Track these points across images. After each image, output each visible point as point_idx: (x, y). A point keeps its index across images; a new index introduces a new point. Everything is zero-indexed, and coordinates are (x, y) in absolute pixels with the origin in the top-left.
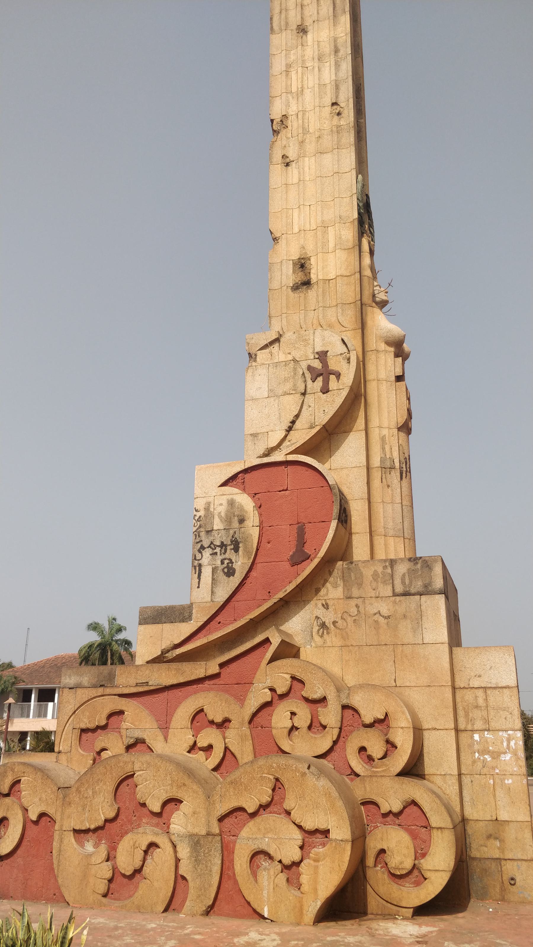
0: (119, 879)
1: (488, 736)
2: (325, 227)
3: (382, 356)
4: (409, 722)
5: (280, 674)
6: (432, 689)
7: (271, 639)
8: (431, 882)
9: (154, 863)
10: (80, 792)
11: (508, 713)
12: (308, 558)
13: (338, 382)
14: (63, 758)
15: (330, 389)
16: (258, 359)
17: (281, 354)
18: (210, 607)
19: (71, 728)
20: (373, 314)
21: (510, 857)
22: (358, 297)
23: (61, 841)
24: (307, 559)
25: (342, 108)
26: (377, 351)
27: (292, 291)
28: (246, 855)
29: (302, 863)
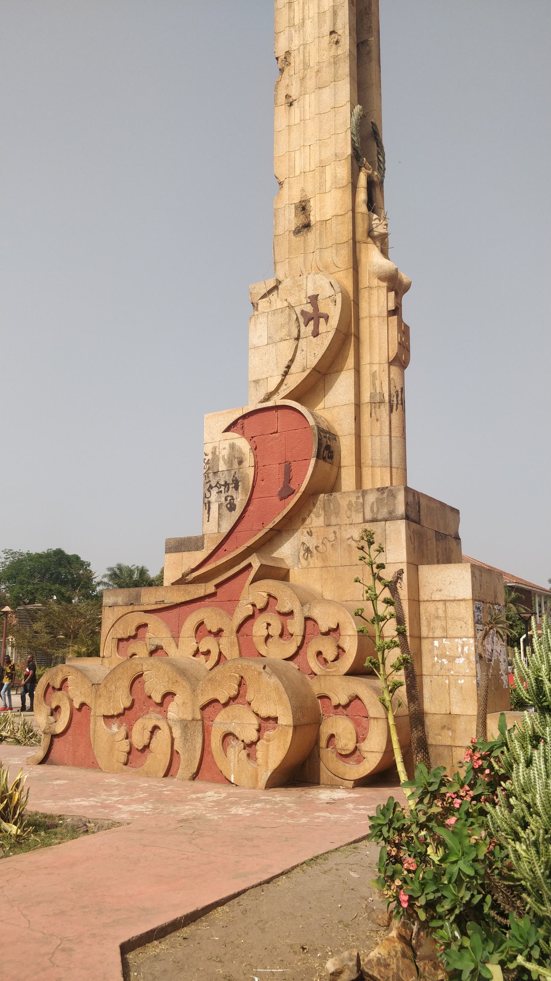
0: (135, 752)
1: (446, 642)
2: (322, 166)
3: (375, 292)
7: (252, 564)
12: (293, 492)
14: (106, 661)
16: (259, 308)
18: (217, 537)
19: (111, 638)
21: (460, 745)
23: (95, 724)
26: (370, 288)
27: (295, 235)
29: (258, 743)
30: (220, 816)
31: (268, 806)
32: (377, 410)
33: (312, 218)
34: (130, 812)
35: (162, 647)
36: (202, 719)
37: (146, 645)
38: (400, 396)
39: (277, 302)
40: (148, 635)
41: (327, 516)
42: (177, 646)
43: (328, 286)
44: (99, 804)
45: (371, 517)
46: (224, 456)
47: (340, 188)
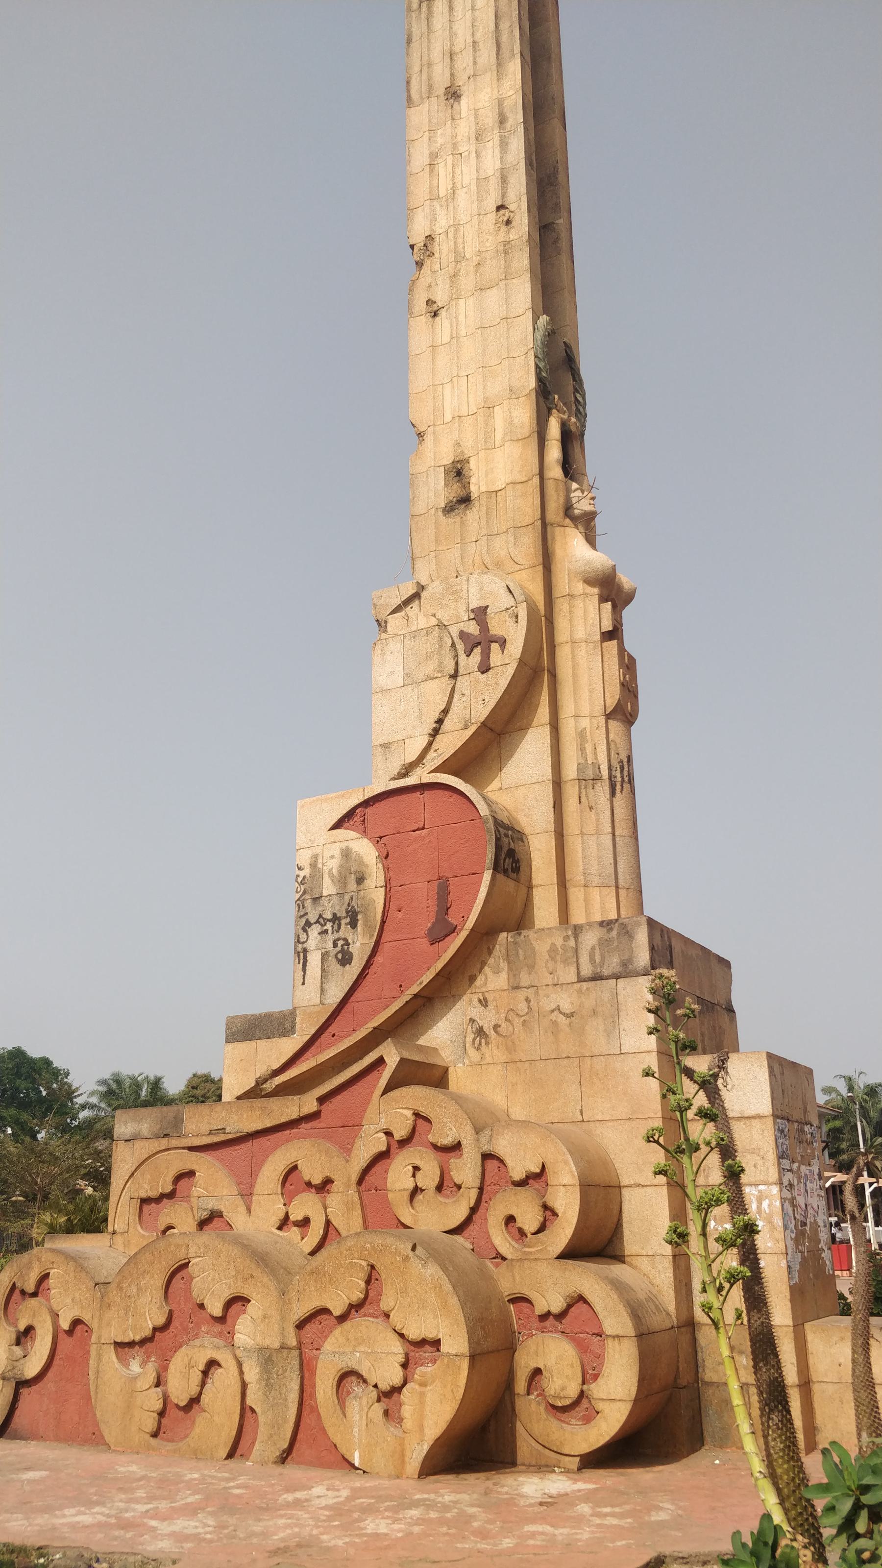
0: (172, 1412)
2: (488, 407)
3: (579, 603)
4: (573, 1176)
5: (398, 1110)
6: (634, 1123)
7: (385, 1058)
8: (604, 1417)
9: (214, 1389)
10: (121, 1289)
11: (758, 1158)
12: (453, 930)
14: (118, 1239)
15: (492, 666)
16: (389, 629)
17: (421, 616)
19: (128, 1198)
22: (538, 514)
24: (452, 933)
25: (512, 212)
26: (571, 596)
28: (332, 1377)
29: (404, 1389)
30: (347, 1540)
31: (433, 1515)
32: (590, 791)
33: (473, 488)
34: (172, 1534)
35: (221, 1212)
36: (299, 1347)
37: (192, 1211)
38: (626, 769)
40: (197, 1191)
41: (513, 972)
42: (249, 1210)
43: (503, 592)
44: (113, 1521)
46: (331, 870)
47: (518, 440)
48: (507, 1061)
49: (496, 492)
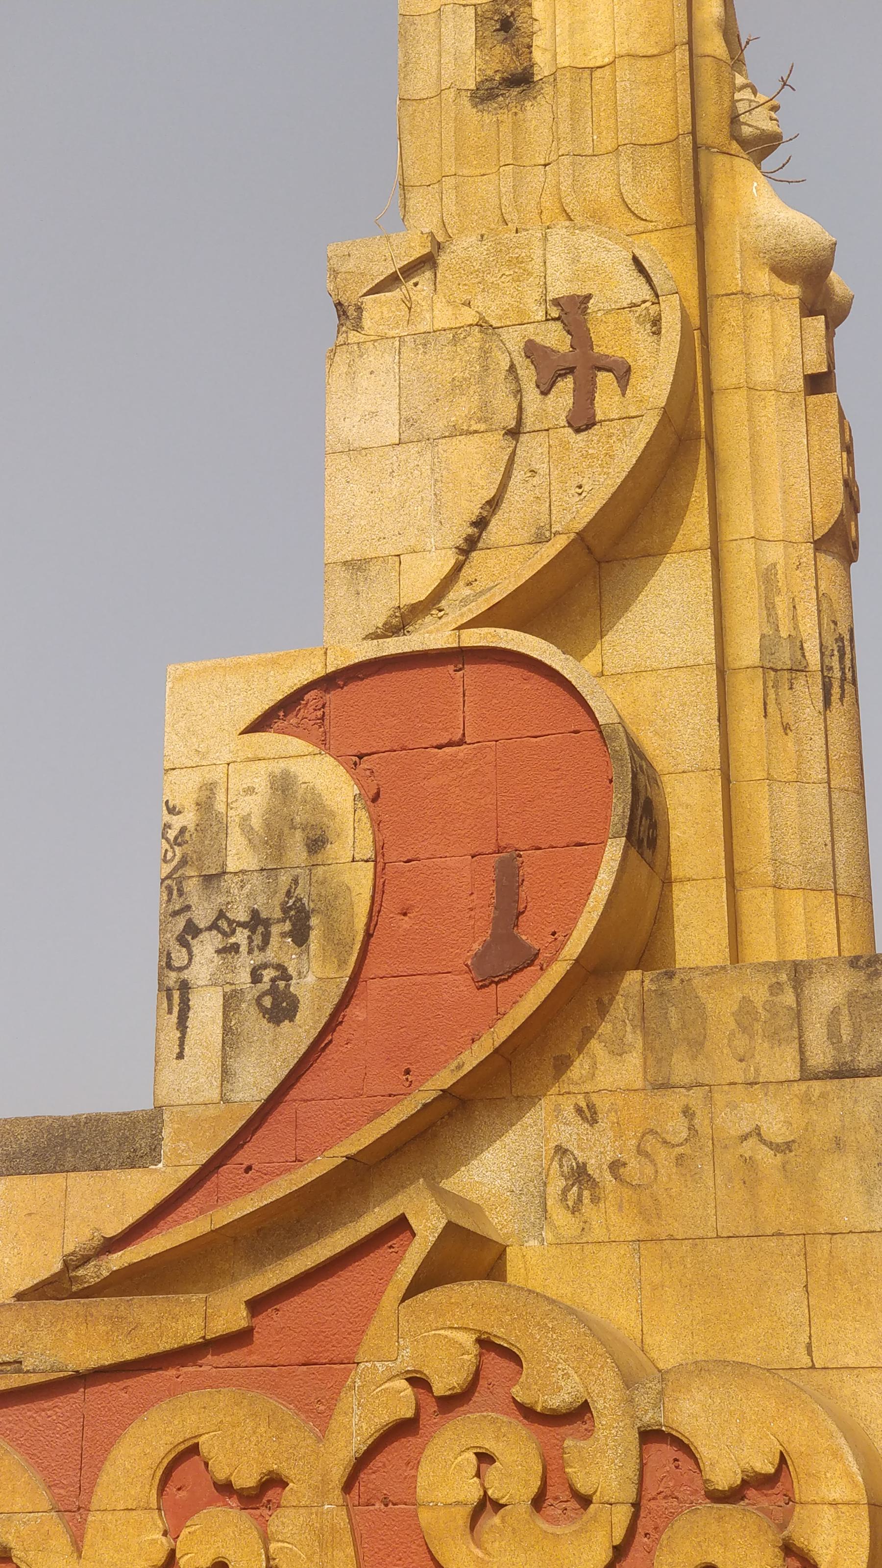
3: (762, 312)
4: (855, 1485)
5: (442, 1332)
7: (412, 1221)
13: (624, 395)
15: (598, 418)
16: (367, 323)
17: (440, 304)
20: (734, 178)
22: (685, 125)
24: (529, 965)
27: (475, 106)
32: (785, 692)
33: (538, 56)
39: (438, 306)
42: (77, 1545)
45: (829, 1060)
48: (642, 1237)
49: (592, 69)
